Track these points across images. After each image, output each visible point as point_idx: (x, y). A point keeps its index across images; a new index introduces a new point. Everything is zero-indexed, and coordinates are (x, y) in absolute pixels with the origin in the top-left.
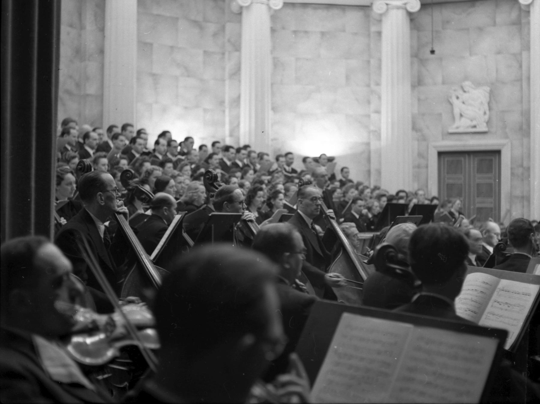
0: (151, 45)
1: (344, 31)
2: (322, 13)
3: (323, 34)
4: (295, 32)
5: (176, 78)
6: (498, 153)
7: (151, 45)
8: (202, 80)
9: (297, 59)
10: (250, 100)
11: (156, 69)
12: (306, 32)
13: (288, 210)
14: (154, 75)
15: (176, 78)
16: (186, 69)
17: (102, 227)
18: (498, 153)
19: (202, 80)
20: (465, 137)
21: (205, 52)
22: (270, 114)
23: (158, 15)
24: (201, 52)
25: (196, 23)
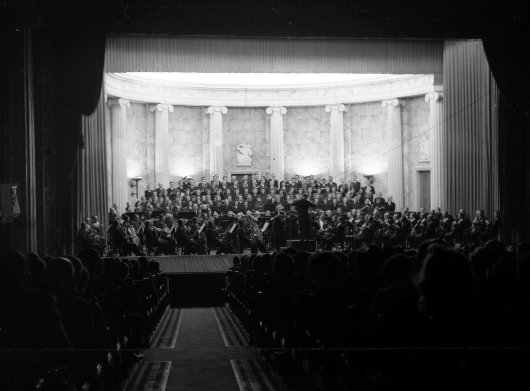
0: (297, 132)
1: (381, 114)
2: (371, 106)
3: (372, 116)
4: (361, 117)
5: (308, 144)
6: (429, 172)
7: (297, 132)
8: (319, 144)
9: (362, 130)
10: (122, 191)
11: (299, 142)
12: (365, 116)
13: (283, 196)
14: (298, 145)
15: (308, 144)
16: (313, 140)
17: (444, 240)
18: (429, 172)
19: (319, 144)
20: (425, 164)
21: (321, 131)
22: (350, 156)
23: (300, 119)
24: (319, 131)
25: (317, 119)
